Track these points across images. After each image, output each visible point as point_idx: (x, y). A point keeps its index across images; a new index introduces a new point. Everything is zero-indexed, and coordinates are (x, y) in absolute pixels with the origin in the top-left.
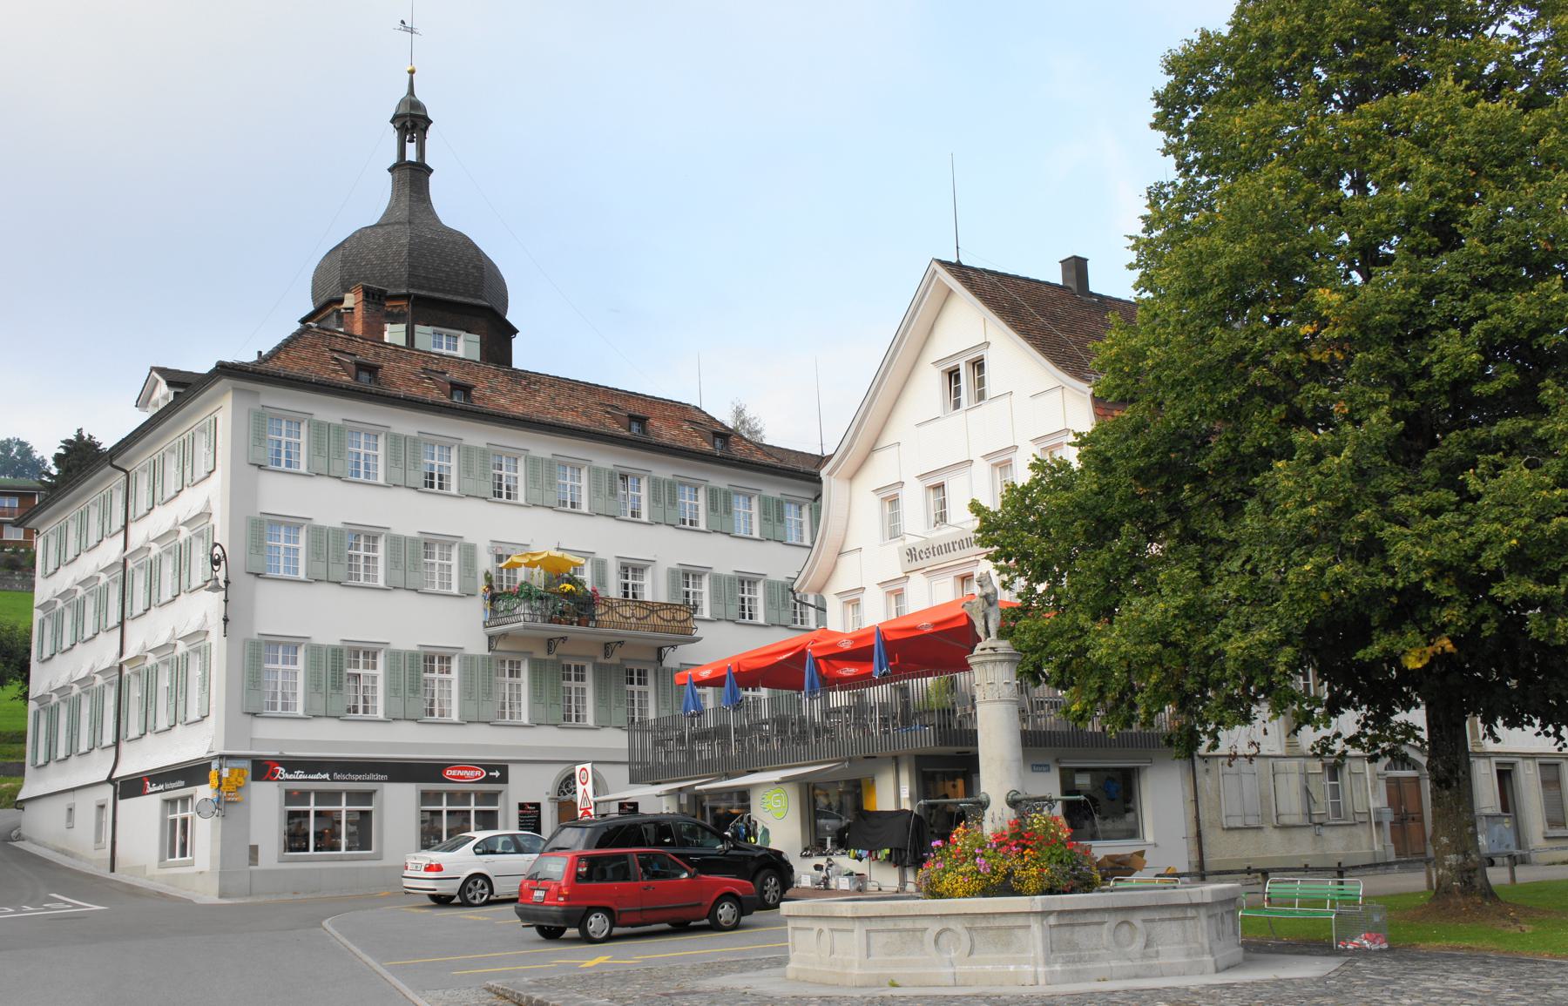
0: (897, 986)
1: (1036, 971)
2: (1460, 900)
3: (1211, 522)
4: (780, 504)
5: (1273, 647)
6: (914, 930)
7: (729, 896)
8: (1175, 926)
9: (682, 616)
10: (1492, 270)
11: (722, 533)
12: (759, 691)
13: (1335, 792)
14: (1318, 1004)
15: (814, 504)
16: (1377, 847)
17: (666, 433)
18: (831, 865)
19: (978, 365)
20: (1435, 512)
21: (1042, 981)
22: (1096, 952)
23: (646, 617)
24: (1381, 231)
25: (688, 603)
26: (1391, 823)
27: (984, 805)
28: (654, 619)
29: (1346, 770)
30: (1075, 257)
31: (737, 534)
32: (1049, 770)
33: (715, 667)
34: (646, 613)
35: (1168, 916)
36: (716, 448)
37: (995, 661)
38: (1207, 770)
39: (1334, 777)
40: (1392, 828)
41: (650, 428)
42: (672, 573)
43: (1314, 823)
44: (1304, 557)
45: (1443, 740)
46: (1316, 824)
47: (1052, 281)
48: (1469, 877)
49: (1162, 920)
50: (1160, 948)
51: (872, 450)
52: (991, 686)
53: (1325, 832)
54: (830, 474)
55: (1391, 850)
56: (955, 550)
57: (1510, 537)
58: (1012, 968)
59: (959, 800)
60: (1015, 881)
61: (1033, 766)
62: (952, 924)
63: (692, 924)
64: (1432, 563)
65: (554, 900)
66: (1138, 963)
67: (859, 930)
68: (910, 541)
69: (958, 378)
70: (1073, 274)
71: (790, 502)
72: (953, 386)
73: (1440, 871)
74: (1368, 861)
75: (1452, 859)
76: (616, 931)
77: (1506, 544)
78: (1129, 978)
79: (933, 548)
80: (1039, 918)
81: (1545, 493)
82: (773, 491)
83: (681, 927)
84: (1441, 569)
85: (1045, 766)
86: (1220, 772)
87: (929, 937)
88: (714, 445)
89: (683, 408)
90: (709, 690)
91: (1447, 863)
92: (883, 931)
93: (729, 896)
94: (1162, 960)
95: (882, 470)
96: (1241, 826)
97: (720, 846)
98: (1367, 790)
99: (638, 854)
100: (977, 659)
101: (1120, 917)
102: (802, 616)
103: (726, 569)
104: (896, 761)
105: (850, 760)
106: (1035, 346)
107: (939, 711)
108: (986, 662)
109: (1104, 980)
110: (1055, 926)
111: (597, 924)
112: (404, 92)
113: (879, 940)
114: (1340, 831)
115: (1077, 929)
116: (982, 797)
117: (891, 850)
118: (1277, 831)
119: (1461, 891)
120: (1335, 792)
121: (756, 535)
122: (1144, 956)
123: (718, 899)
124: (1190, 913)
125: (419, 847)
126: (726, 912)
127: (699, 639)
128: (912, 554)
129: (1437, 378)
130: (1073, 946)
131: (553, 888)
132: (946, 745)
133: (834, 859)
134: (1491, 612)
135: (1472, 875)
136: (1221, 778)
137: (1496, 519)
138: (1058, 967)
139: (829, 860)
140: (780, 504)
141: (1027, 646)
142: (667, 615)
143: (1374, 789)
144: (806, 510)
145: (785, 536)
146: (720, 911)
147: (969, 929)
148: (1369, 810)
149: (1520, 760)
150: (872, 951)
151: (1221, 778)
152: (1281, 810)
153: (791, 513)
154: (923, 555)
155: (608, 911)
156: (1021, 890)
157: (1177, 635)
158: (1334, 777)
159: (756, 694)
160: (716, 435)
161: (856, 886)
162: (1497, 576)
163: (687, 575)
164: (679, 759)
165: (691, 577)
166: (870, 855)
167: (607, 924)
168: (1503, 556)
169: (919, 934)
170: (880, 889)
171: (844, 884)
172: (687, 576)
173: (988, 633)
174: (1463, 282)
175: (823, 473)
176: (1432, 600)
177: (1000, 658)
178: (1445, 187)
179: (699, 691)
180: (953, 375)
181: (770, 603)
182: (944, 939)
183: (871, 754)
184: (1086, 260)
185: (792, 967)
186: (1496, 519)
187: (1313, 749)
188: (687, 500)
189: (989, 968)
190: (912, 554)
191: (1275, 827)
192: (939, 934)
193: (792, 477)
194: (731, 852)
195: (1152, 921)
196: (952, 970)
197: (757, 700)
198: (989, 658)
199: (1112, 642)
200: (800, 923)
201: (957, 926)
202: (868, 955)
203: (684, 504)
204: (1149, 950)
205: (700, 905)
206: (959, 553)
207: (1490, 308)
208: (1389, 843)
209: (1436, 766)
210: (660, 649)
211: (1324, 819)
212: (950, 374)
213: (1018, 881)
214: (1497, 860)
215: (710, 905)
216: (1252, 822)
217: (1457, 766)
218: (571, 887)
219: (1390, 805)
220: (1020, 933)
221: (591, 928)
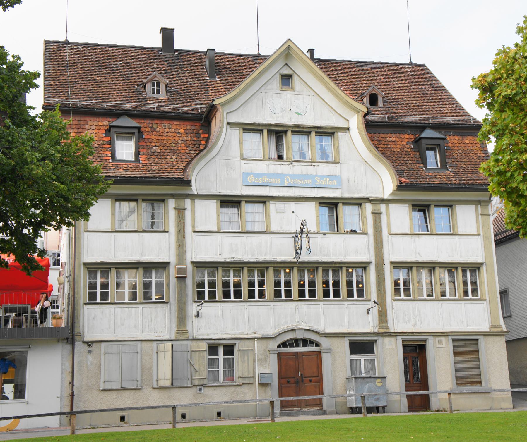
53: (205, 390)
86: (103, 352)
98: (254, 361)
112: (258, 52)
118: (156, 391)
136: (103, 356)
151: (103, 356)
184: (173, 30)
211: (205, 382)
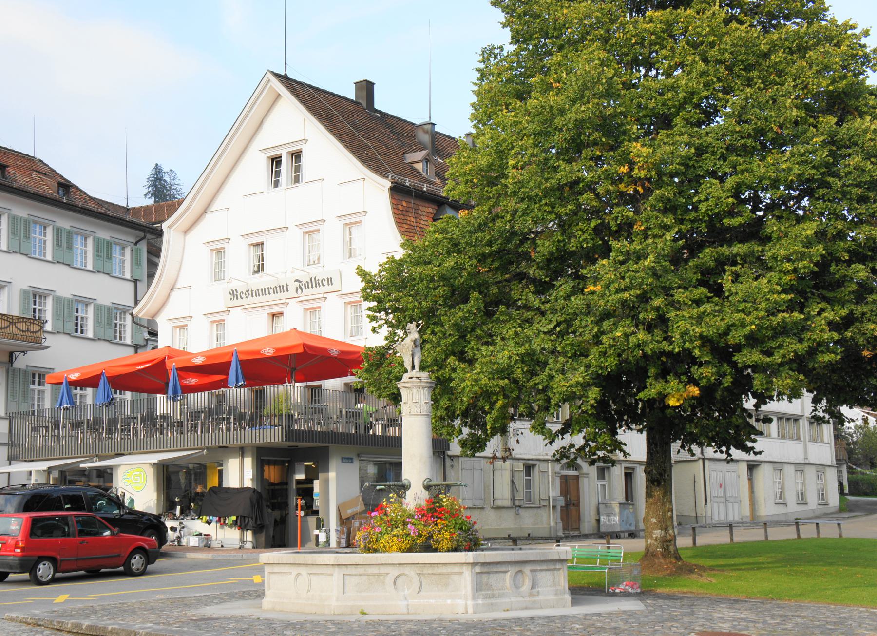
1: (466, 604)
2: (662, 561)
3: (526, 295)
4: (109, 244)
5: (585, 386)
6: (379, 575)
7: (140, 550)
8: (548, 574)
9: (34, 328)
10: (742, 142)
11: (63, 263)
12: (85, 390)
13: (528, 484)
14: (487, 634)
15: (135, 247)
16: (552, 524)
17: (21, 180)
18: (183, 527)
19: (297, 156)
20: (698, 302)
21: (470, 611)
22: (501, 591)
23: (7, 328)
24: (668, 105)
25: (34, 316)
26: (561, 507)
27: (405, 488)
28: (12, 329)
29: (537, 468)
30: (367, 81)
31: (75, 266)
32: (352, 462)
33: (84, 371)
34: (6, 324)
35: (545, 567)
36: (60, 195)
38: (452, 466)
39: (528, 474)
40: (562, 510)
41: (7, 174)
42: (24, 293)
43: (515, 506)
44: (612, 326)
45: (658, 453)
46: (516, 506)
47: (349, 97)
48: (667, 545)
49: (541, 570)
51: (205, 211)
52: (415, 404)
53: (521, 511)
54: (170, 227)
55: (560, 526)
56: (269, 294)
57: (752, 323)
58: (449, 602)
59: (391, 483)
60: (433, 541)
61: (342, 458)
62: (407, 570)
63: (103, 570)
64: (701, 337)
65: (10, 551)
66: (527, 599)
67: (338, 574)
68: (234, 285)
69: (279, 163)
70: (364, 93)
71: (116, 244)
72: (274, 170)
73: (649, 541)
74: (546, 535)
75: (658, 533)
76: (58, 575)
77: (748, 328)
78: (523, 609)
79: (252, 291)
80: (470, 567)
81: (775, 296)
82: (105, 233)
83: (94, 574)
84: (705, 340)
85: (351, 458)
87: (389, 580)
88: (58, 193)
89: (30, 159)
90: (89, 391)
91: (654, 536)
92: (356, 575)
93: (140, 550)
94: (541, 598)
95: (208, 227)
96: (471, 506)
97: (116, 512)
99: (76, 516)
100: (404, 385)
101: (517, 568)
102: (120, 333)
103: (66, 292)
104: (242, 451)
105: (208, 448)
106: (347, 147)
107: (285, 415)
108: (413, 387)
109: (507, 610)
110: (479, 573)
111: (45, 570)
113: (352, 581)
114: (531, 511)
115: (491, 575)
116: (405, 482)
117: (237, 517)
118: (493, 510)
119: (663, 555)
120: (528, 484)
121: (90, 267)
122: (531, 595)
123: (132, 551)
124: (558, 566)
125: (22, 509)
126: (137, 562)
127: (47, 347)
128: (234, 294)
129: (702, 211)
131: (10, 541)
132: (289, 441)
133: (185, 522)
134: (729, 371)
135: (669, 544)
137: (743, 311)
138: (480, 602)
139: (181, 523)
140: (109, 244)
141: (395, 376)
142: (23, 326)
143: (553, 482)
144: (128, 251)
145: (112, 270)
146: (133, 561)
147: (419, 574)
148: (549, 497)
149: (638, 466)
150: (347, 589)
152: (496, 496)
153: (116, 251)
154: (243, 296)
155: (53, 560)
156: (437, 548)
157: (518, 374)
158: (528, 474)
159: (122, 396)
160: (60, 185)
161: (204, 543)
162: (738, 348)
163: (36, 295)
164: (50, 442)
165: (38, 297)
166: (219, 521)
167: (52, 570)
168: (745, 336)
169: (382, 577)
170: (222, 546)
171: (194, 541)
172: (35, 296)
173: (413, 368)
174: (722, 148)
175: (165, 226)
176: (694, 361)
177: (423, 384)
178: (712, 80)
179: (78, 391)
180: (276, 161)
181: (98, 322)
182: (399, 581)
185: (267, 602)
186: (743, 311)
187: (555, 455)
188: (37, 236)
189: (432, 601)
190: (234, 294)
191: (492, 508)
192: (397, 577)
193: (121, 224)
194: (126, 517)
195: (535, 571)
196: (406, 603)
197: (123, 401)
198: (415, 384)
199: (474, 377)
200: (276, 569)
201: (411, 572)
202: (344, 592)
203: (35, 238)
204: (534, 590)
205: (119, 556)
206: (273, 296)
207: (738, 168)
208: (559, 521)
209: (652, 470)
210: (11, 354)
211: (521, 503)
212: (273, 160)
213: (436, 541)
214: (622, 535)
215: (126, 556)
216: (479, 504)
217: (665, 471)
218: (26, 540)
219: (561, 494)
220: (456, 577)
221: (39, 573)
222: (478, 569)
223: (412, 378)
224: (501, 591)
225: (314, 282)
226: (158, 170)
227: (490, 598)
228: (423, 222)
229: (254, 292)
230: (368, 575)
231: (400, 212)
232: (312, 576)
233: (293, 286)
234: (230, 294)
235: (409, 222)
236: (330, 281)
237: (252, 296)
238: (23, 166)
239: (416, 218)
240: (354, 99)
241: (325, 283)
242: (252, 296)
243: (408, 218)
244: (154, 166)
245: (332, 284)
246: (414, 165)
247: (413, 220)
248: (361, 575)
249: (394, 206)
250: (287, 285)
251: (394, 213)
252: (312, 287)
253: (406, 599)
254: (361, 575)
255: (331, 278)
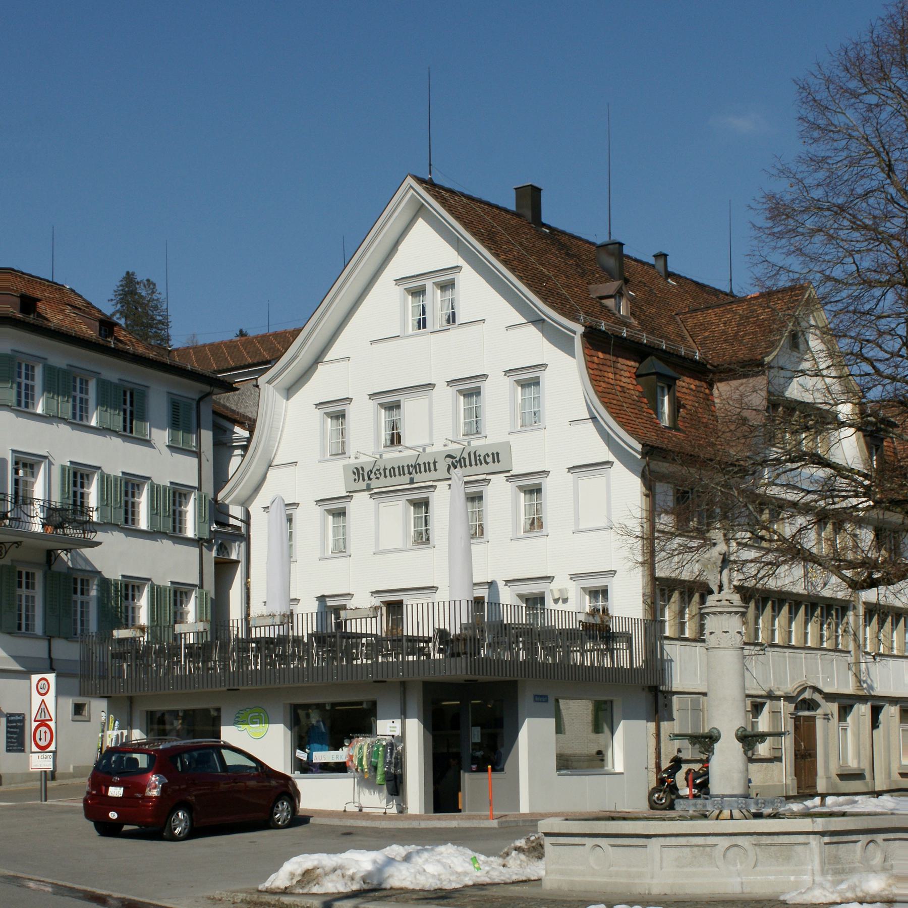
0: (209, 898)
6: (704, 846)
17: (56, 318)
37: (730, 613)
50: (893, 862)
51: (318, 360)
54: (269, 382)
62: (740, 840)
79: (385, 469)
87: (719, 852)
92: (676, 846)
101: (869, 837)
103: (115, 470)
128: (359, 473)
130: (836, 859)
169: (708, 849)
183: (380, 679)
189: (772, 878)
192: (728, 849)
196: (739, 879)
202: (661, 868)
220: (799, 849)
222: (827, 839)
223: (720, 601)
224: (852, 865)
225: (477, 459)
226: (129, 279)
227: (839, 873)
228: (624, 380)
229: (387, 472)
230: (691, 846)
231: (595, 366)
232: (664, 849)
233: (442, 465)
234: (354, 473)
235: (606, 379)
236: (496, 457)
237: (385, 476)
238: (53, 298)
239: (615, 374)
240: (512, 207)
241: (490, 460)
242: (385, 476)
243: (606, 374)
244: (124, 274)
245: (499, 461)
246: (604, 301)
247: (611, 376)
248: (682, 846)
249: (588, 358)
250: (435, 462)
251: (588, 368)
252: (471, 465)
253: (739, 875)
254: (682, 846)
255: (498, 454)
